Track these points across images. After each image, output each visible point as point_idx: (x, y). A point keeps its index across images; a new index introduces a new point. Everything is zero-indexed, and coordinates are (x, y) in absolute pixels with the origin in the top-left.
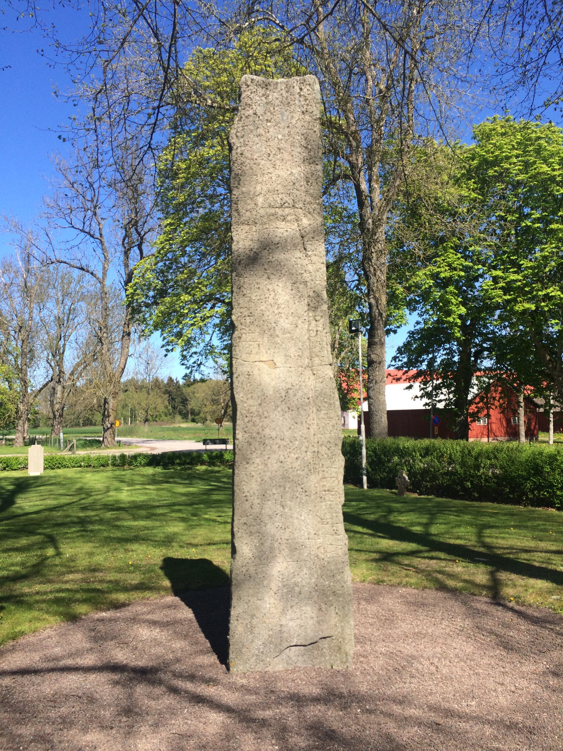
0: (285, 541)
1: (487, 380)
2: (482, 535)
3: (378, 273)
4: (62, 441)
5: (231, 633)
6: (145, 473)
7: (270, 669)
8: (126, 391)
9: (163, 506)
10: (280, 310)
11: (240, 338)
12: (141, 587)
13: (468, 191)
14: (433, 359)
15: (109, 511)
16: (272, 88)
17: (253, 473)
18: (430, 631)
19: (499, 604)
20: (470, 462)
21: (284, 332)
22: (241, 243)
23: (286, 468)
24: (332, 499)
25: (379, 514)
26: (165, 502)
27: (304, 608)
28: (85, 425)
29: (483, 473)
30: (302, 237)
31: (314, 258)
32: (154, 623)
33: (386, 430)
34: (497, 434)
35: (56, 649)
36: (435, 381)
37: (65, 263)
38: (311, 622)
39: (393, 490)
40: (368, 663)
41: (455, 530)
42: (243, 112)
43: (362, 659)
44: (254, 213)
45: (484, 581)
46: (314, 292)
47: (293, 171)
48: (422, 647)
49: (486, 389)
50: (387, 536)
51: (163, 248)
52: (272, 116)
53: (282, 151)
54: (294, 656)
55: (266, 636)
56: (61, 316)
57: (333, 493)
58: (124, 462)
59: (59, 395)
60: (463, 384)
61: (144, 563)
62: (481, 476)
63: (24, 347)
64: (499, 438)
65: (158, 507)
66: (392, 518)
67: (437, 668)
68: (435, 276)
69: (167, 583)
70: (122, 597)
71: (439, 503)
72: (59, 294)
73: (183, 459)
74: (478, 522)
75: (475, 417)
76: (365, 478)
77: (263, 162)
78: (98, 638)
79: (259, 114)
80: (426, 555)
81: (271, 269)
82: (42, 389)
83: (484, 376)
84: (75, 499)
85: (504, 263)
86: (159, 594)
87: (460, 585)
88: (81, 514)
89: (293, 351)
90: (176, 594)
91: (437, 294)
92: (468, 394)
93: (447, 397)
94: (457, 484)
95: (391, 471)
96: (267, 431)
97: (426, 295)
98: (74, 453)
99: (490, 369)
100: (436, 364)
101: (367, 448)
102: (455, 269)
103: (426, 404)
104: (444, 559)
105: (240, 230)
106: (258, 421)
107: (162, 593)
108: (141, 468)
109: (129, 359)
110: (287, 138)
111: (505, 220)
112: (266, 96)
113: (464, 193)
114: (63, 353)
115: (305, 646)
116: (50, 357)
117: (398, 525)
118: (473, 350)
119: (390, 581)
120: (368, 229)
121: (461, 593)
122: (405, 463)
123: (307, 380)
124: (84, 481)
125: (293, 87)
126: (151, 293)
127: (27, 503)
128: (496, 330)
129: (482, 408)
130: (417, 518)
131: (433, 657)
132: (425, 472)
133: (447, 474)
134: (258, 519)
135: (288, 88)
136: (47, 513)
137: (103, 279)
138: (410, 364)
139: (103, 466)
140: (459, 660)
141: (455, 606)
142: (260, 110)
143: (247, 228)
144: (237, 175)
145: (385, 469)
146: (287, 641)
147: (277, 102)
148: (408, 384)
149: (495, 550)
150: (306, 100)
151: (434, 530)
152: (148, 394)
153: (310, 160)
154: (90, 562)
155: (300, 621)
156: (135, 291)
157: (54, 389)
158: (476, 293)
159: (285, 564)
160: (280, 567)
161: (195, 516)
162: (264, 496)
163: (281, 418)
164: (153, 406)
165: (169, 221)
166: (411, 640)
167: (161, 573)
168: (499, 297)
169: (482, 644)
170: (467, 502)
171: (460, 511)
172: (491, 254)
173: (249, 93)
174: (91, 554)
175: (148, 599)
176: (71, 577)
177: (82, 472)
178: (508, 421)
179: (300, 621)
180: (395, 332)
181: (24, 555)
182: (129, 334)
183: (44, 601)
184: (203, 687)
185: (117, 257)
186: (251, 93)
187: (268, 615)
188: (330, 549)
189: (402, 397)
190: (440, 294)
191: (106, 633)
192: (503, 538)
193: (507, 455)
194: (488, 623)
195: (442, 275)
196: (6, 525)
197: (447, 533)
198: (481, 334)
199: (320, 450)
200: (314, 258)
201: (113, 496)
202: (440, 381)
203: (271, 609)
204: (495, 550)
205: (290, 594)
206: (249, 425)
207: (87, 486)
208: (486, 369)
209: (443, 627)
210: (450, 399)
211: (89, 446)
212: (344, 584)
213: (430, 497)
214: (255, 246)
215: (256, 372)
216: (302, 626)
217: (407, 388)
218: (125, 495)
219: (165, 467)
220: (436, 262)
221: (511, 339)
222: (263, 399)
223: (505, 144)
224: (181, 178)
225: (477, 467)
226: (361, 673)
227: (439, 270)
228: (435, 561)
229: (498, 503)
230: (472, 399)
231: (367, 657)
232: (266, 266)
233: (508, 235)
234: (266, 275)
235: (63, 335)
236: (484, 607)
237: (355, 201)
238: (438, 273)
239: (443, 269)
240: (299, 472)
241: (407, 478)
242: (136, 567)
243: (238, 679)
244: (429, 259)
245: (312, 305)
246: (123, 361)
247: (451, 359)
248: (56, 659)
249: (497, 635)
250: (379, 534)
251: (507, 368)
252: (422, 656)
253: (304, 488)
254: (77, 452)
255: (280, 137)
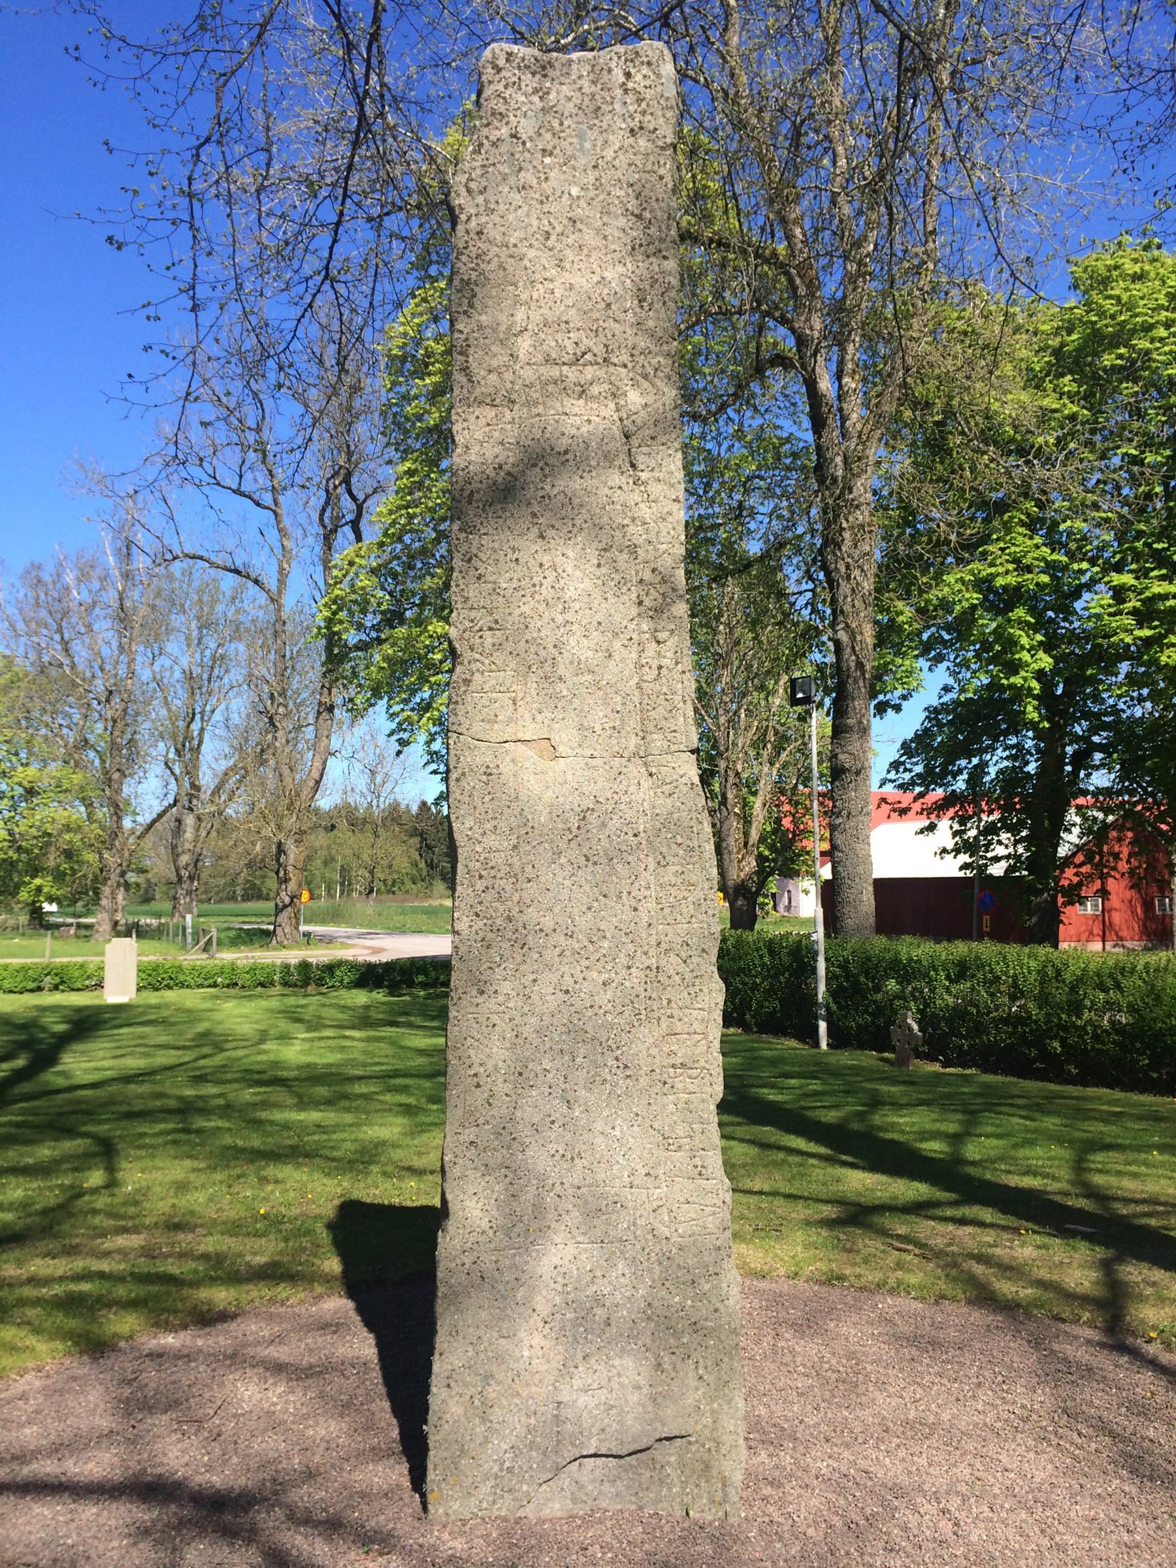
0: (571, 1191)
1: (1100, 815)
2: (1085, 1165)
3: (856, 573)
4: (189, 930)
5: (432, 1417)
6: (349, 1002)
7: (529, 1512)
8: (333, 827)
9: (371, 1077)
10: (569, 616)
11: (467, 682)
12: (273, 1273)
13: (1061, 399)
14: (982, 767)
15: (250, 1086)
16: (558, 73)
17: (495, 1019)
18: (946, 1416)
19: (1122, 1348)
20: (1060, 995)
21: (580, 667)
22: (475, 449)
23: (579, 1005)
24: (691, 1088)
25: (848, 1109)
26: (378, 1068)
27: (617, 1362)
28: (246, 898)
29: (1089, 1022)
30: (627, 437)
31: (655, 489)
32: (278, 1368)
33: (872, 920)
34: (1124, 933)
35: (27, 1431)
36: (984, 817)
37: (201, 558)
38: (634, 1398)
39: (886, 1055)
40: (782, 1503)
41: (1021, 1153)
42: (485, 131)
43: (768, 1491)
44: (508, 376)
45: (1087, 1284)
46: (654, 570)
47: (606, 274)
48: (923, 1461)
49: (1098, 834)
50: (861, 1163)
51: (394, 523)
52: (556, 141)
53: (579, 225)
54: (592, 1481)
55: (521, 1430)
56: (197, 671)
57: (694, 1072)
58: (306, 977)
59: (189, 834)
60: (1046, 823)
61: (295, 1211)
62: (1084, 1028)
63: (116, 733)
64: (1128, 944)
65: (360, 1078)
66: (877, 1119)
67: (956, 1524)
68: (983, 585)
69: (333, 1265)
70: (221, 1296)
71: (986, 1086)
72: (194, 625)
73: (433, 974)
74: (1078, 1134)
75: (1074, 895)
76: (823, 1026)
77: (532, 253)
78: (137, 1405)
79: (524, 137)
80: (949, 1212)
81: (548, 514)
82: (154, 821)
83: (1094, 806)
84: (188, 1056)
85: (1138, 556)
86: (312, 1290)
87: (1027, 1293)
88: (189, 1092)
89: (598, 717)
90: (351, 1295)
91: (988, 624)
92: (1058, 845)
93: (1011, 850)
94: (1030, 1044)
95: (880, 1011)
96: (532, 914)
97: (963, 626)
98: (212, 957)
99: (1107, 792)
100: (987, 779)
101: (827, 960)
102: (1029, 569)
103: (965, 867)
104: (992, 1226)
105: (472, 418)
106: (508, 888)
107: (319, 1290)
108: (343, 992)
109: (331, 762)
110: (592, 193)
111: (1141, 463)
112: (544, 94)
113: (1051, 402)
114: (199, 745)
115: (620, 1457)
116: (171, 755)
117: (889, 1136)
118: (1069, 750)
119: (859, 1276)
120: (834, 480)
121: (1028, 1315)
122: (912, 994)
123: (632, 789)
124: (217, 1016)
125: (610, 71)
126: (370, 620)
127: (82, 1064)
128: (1121, 706)
129: (1089, 876)
130: (934, 1121)
131: (948, 1493)
132: (958, 1014)
133: (1005, 1021)
134: (507, 1134)
135: (598, 73)
136: (115, 1088)
137: (280, 592)
138: (929, 778)
139: (262, 985)
140: (1013, 1501)
141: (1014, 1350)
142: (526, 128)
143: (490, 413)
144: (468, 282)
145: (868, 1006)
146: (573, 1444)
147: (570, 108)
148: (927, 823)
149: (1117, 1205)
150: (639, 101)
151: (972, 1150)
152: (377, 836)
153: (647, 249)
154: (174, 1206)
155: (608, 1392)
156: (335, 613)
157: (179, 821)
158: (1076, 624)
159: (571, 1249)
160: (561, 1256)
161: (435, 1103)
162: (521, 1076)
163: (567, 883)
164: (385, 862)
165: (408, 465)
166: (896, 1441)
167: (324, 1236)
168: (1129, 632)
169: (1075, 1458)
170: (1052, 1087)
171: (1037, 1108)
172: (1108, 537)
173: (500, 87)
174: (181, 1187)
175: (283, 1303)
176: (121, 1241)
177: (217, 997)
178: (1148, 906)
179: (608, 1392)
180: (898, 708)
181: (35, 1185)
182: (331, 709)
183: (38, 1302)
184: (352, 1555)
185: (308, 546)
186: (506, 87)
187: (526, 1376)
188: (687, 1213)
189: (909, 849)
190: (994, 625)
191: (156, 1390)
192: (1135, 1175)
193: (1145, 982)
194: (1097, 1400)
195: (1000, 582)
196: (22, 1112)
197: (1002, 1159)
198: (1087, 715)
199: (663, 963)
200: (655, 489)
201: (275, 1051)
202: (996, 816)
203: (535, 1362)
204: (1117, 1205)
205: (586, 1325)
206: (488, 897)
207: (219, 1029)
208: (1099, 791)
209: (980, 1407)
210: (1017, 857)
211: (244, 943)
212: (718, 1305)
213: (969, 1071)
214: (510, 458)
215: (506, 768)
216: (612, 1407)
217: (922, 832)
218: (296, 1051)
219: (393, 990)
220: (984, 554)
221: (1154, 727)
222: (525, 834)
223: (1142, 298)
224: (435, 374)
225: (1076, 1007)
226: (761, 1532)
227: (993, 570)
228: (969, 1229)
229: (1122, 1090)
230: (1067, 858)
231: (780, 1485)
232: (536, 508)
233: (1149, 496)
234: (535, 530)
235: (198, 710)
236: (1083, 1355)
237: (806, 423)
238: (993, 577)
239: (1001, 570)
240: (609, 1018)
241: (915, 1027)
242: (274, 1222)
243: (446, 1536)
244: (971, 547)
245: (647, 602)
246: (318, 764)
247: (1021, 768)
248: (21, 1458)
249: (1113, 1435)
250: (844, 1157)
251: (1145, 789)
252: (920, 1489)
253: (623, 1059)
254: (218, 955)
255: (575, 191)
